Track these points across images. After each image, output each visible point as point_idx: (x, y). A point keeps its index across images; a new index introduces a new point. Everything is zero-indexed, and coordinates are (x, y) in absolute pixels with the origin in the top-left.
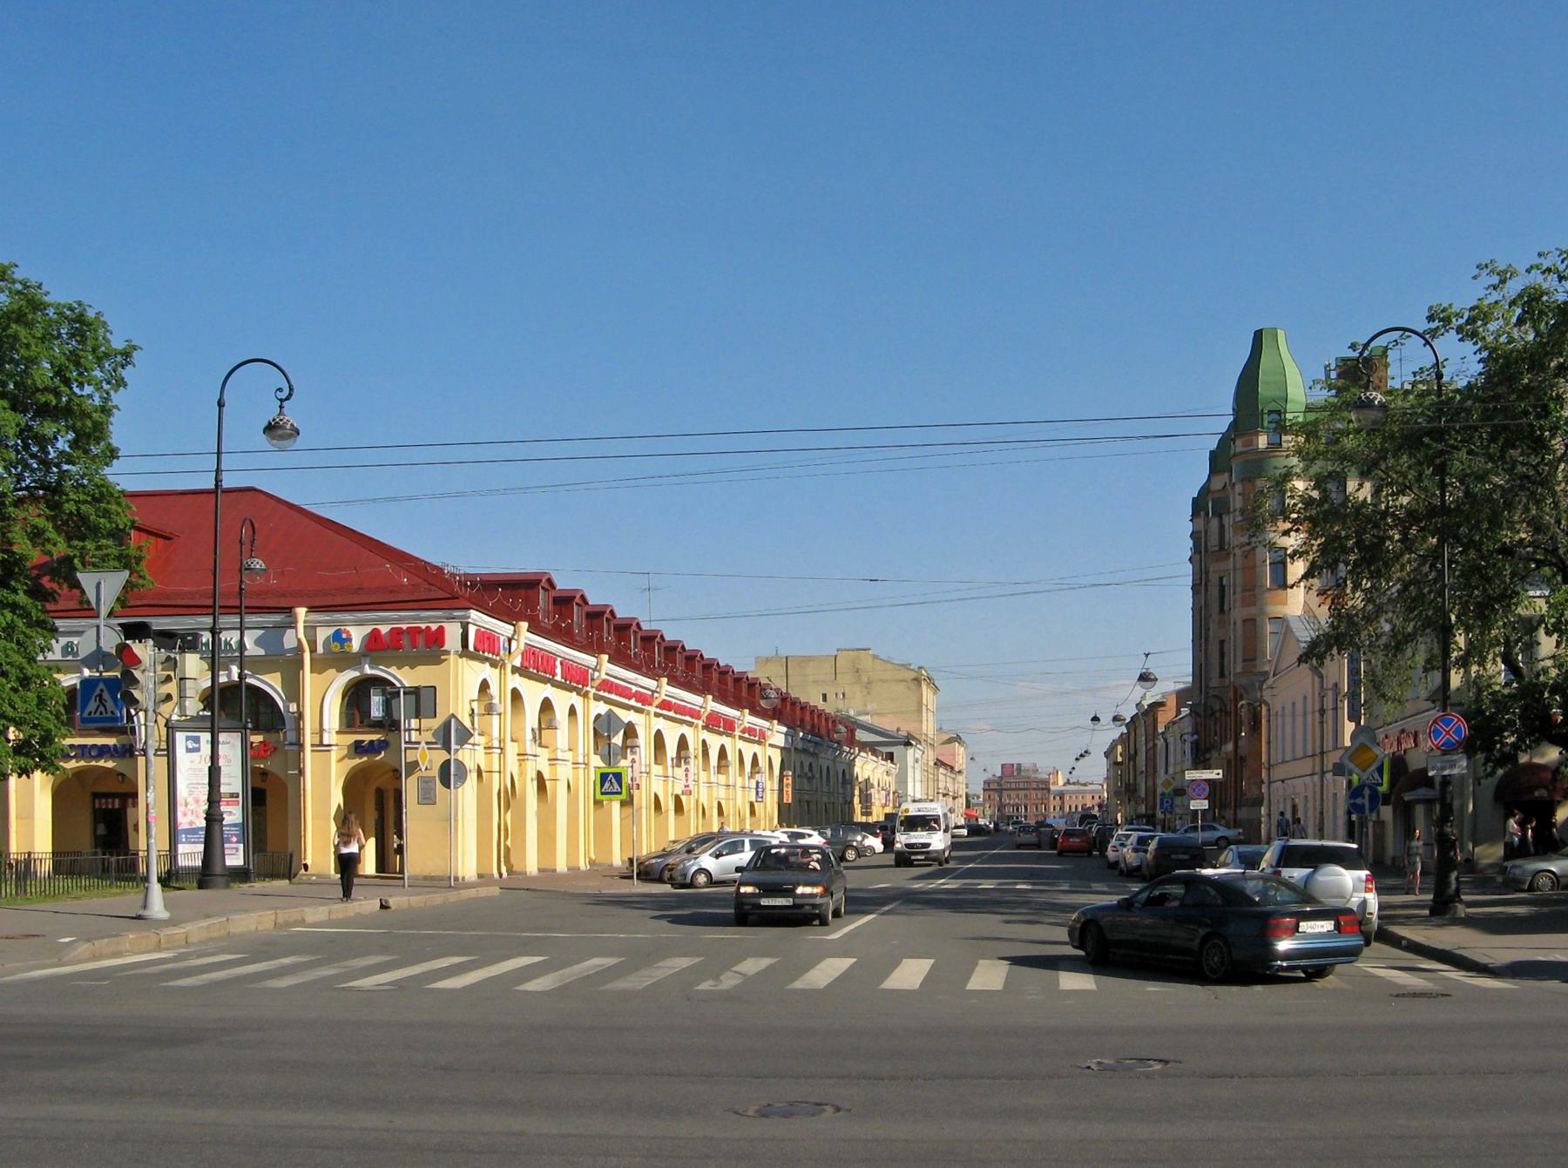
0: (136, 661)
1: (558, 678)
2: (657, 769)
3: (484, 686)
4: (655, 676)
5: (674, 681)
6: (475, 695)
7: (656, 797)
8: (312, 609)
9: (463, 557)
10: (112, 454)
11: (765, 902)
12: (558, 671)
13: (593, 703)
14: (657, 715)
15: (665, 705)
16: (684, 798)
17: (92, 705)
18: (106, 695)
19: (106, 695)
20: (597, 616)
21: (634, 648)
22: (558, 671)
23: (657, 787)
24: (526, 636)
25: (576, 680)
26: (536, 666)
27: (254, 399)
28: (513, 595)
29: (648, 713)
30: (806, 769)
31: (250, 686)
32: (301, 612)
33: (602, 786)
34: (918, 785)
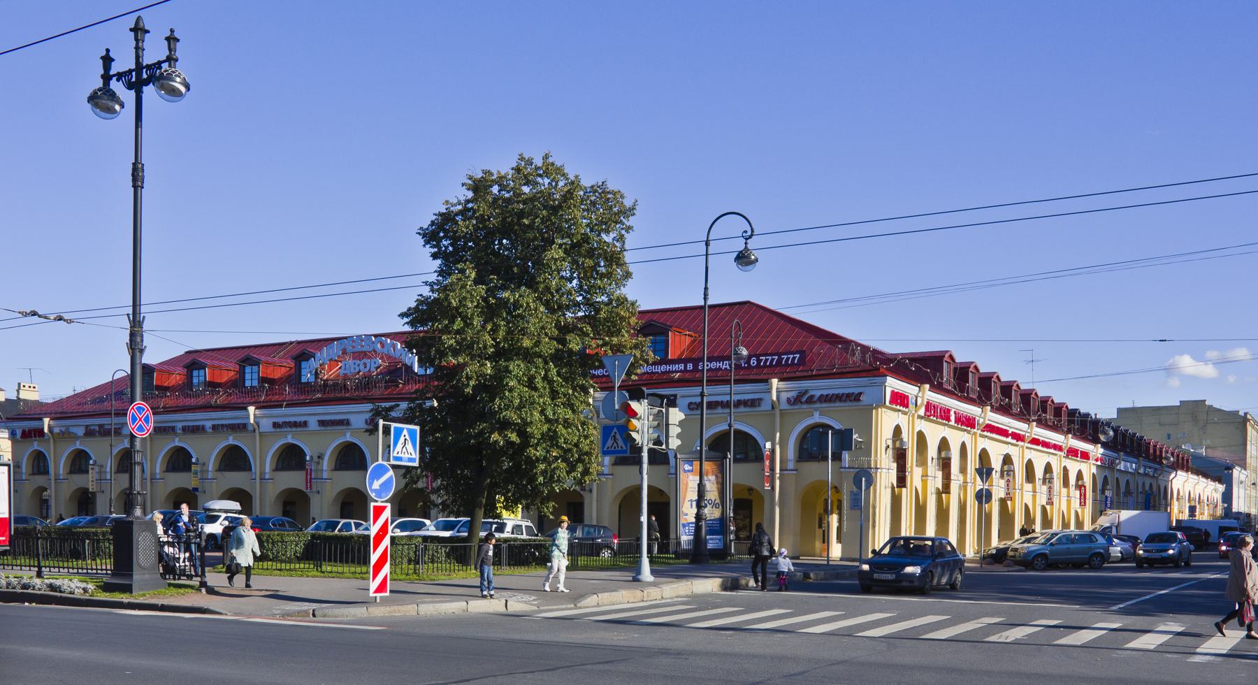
0: (634, 414)
1: (952, 423)
2: (1028, 487)
3: (898, 430)
4: (1028, 421)
5: (1075, 436)
6: (890, 435)
7: (1026, 506)
8: (781, 380)
9: (891, 347)
10: (628, 275)
11: (876, 576)
12: (953, 418)
13: (979, 439)
14: (981, 436)
15: (990, 428)
16: (1048, 507)
17: (610, 443)
18: (618, 436)
19: (618, 436)
20: (986, 381)
21: (1049, 416)
22: (953, 418)
23: (1028, 499)
24: (929, 395)
25: (967, 422)
26: (937, 414)
27: (729, 236)
28: (924, 368)
29: (975, 434)
30: (1147, 488)
31: (737, 432)
32: (775, 381)
33: (604, 442)
34: (1242, 500)
